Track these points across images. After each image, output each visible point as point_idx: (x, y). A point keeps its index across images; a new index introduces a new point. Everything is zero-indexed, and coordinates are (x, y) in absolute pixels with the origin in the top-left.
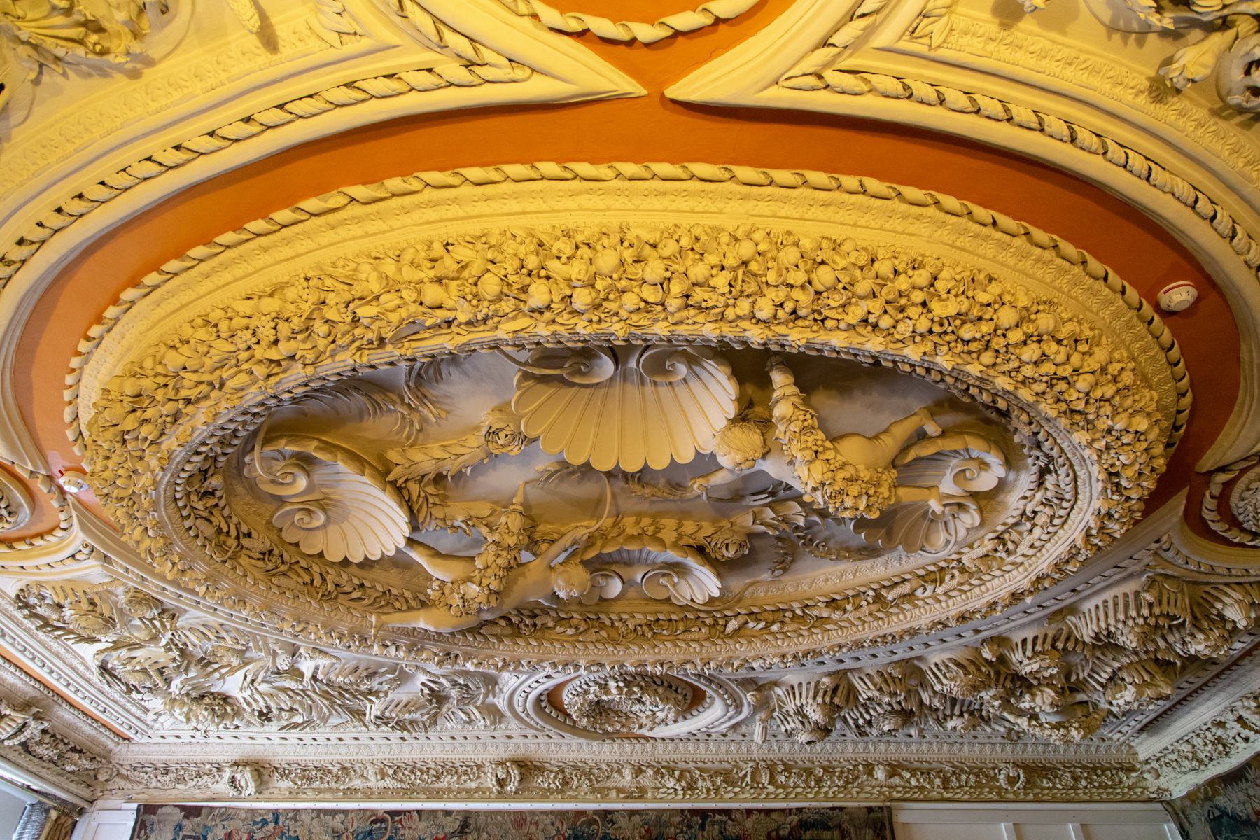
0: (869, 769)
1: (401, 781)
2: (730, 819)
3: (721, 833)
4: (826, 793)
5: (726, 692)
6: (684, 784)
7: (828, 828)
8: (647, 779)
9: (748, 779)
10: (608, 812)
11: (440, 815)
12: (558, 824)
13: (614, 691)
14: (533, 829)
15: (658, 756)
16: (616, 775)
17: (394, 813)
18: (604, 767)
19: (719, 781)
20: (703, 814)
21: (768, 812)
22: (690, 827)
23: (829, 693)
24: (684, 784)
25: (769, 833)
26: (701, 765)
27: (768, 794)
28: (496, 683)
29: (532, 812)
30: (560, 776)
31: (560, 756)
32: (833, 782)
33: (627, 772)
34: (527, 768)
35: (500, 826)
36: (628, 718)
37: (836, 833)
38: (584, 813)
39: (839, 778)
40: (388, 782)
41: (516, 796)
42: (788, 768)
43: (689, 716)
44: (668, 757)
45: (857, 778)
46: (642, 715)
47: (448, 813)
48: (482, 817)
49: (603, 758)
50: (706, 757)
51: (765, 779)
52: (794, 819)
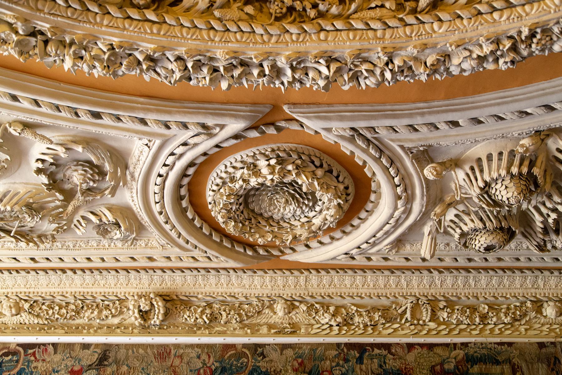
0: (538, 305)
1: (38, 316)
2: (390, 352)
3: (381, 366)
4: (492, 330)
5: (398, 172)
6: (339, 319)
7: (497, 363)
8: (300, 315)
9: (408, 315)
10: (257, 346)
11: (77, 348)
12: (204, 357)
13: (265, 171)
14: (177, 362)
15: (311, 290)
16: (267, 311)
17: (26, 347)
18: (255, 302)
19: (376, 316)
20: (361, 348)
21: (431, 346)
22: (346, 360)
23: (526, 163)
24: (339, 319)
25: (433, 367)
26: (357, 300)
27: (429, 331)
28: (127, 167)
29: (177, 346)
30: (208, 311)
31: (208, 289)
32: (499, 318)
33: (279, 308)
34: (173, 303)
35: (142, 359)
36: (280, 228)
37: (507, 368)
38: (232, 346)
39: (506, 315)
40: (25, 318)
41: (161, 329)
42: (450, 305)
43: (348, 229)
44: (323, 291)
45: (525, 315)
46: (296, 223)
47: (86, 346)
48: (123, 351)
49: (253, 292)
50: (363, 291)
51: (426, 315)
52: (461, 353)
